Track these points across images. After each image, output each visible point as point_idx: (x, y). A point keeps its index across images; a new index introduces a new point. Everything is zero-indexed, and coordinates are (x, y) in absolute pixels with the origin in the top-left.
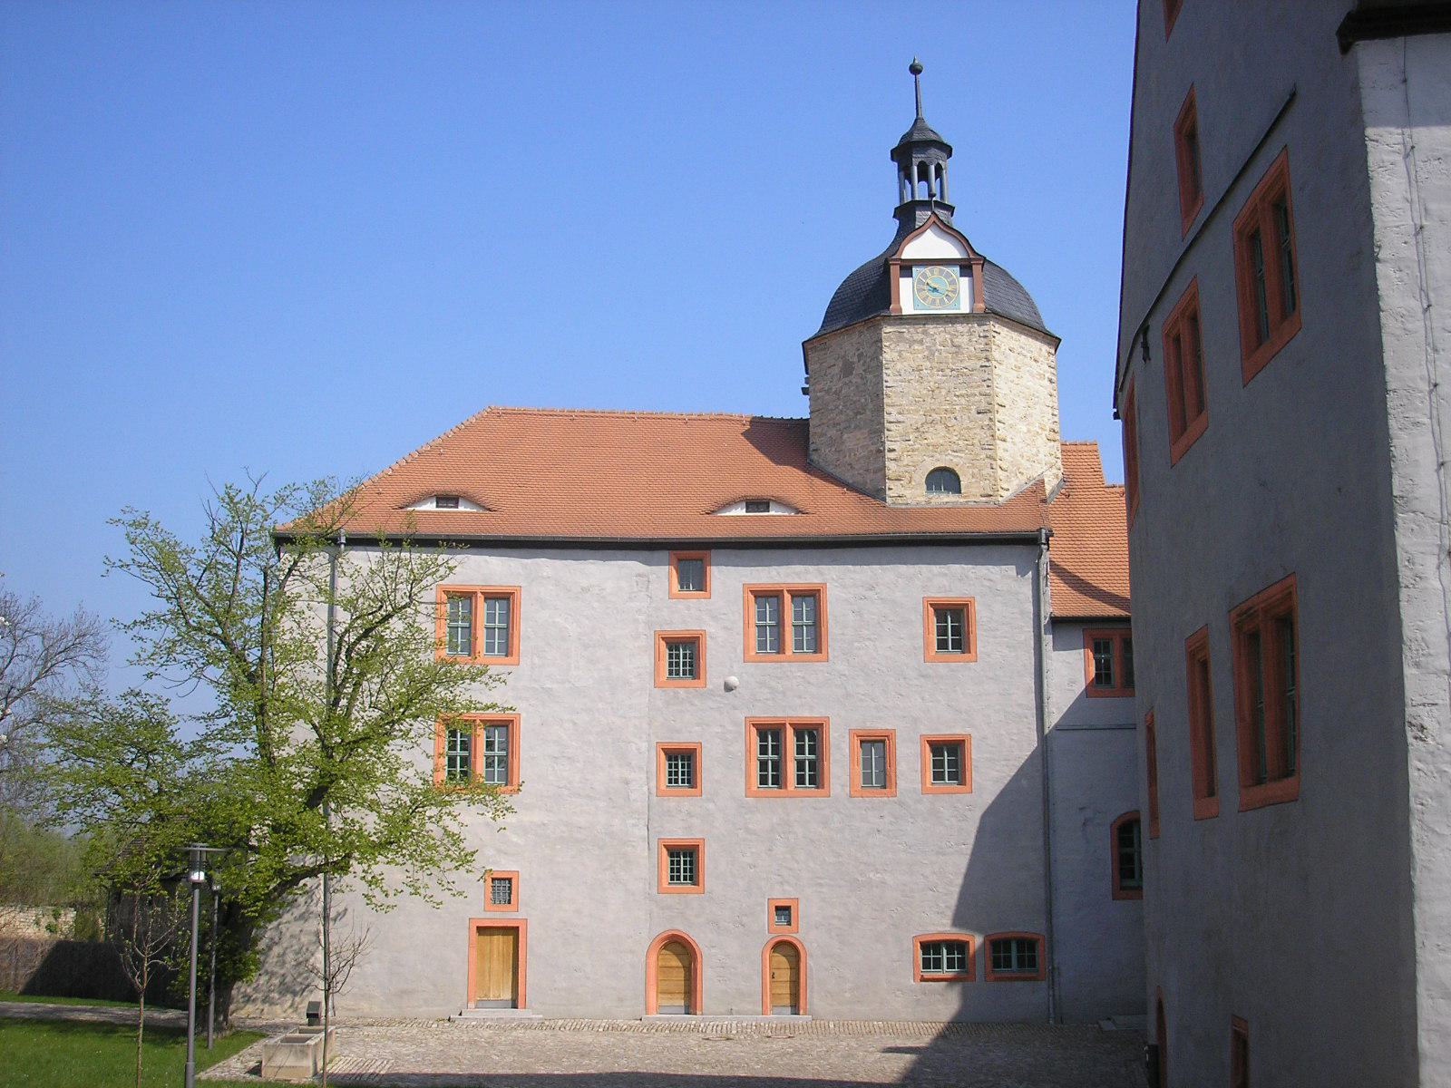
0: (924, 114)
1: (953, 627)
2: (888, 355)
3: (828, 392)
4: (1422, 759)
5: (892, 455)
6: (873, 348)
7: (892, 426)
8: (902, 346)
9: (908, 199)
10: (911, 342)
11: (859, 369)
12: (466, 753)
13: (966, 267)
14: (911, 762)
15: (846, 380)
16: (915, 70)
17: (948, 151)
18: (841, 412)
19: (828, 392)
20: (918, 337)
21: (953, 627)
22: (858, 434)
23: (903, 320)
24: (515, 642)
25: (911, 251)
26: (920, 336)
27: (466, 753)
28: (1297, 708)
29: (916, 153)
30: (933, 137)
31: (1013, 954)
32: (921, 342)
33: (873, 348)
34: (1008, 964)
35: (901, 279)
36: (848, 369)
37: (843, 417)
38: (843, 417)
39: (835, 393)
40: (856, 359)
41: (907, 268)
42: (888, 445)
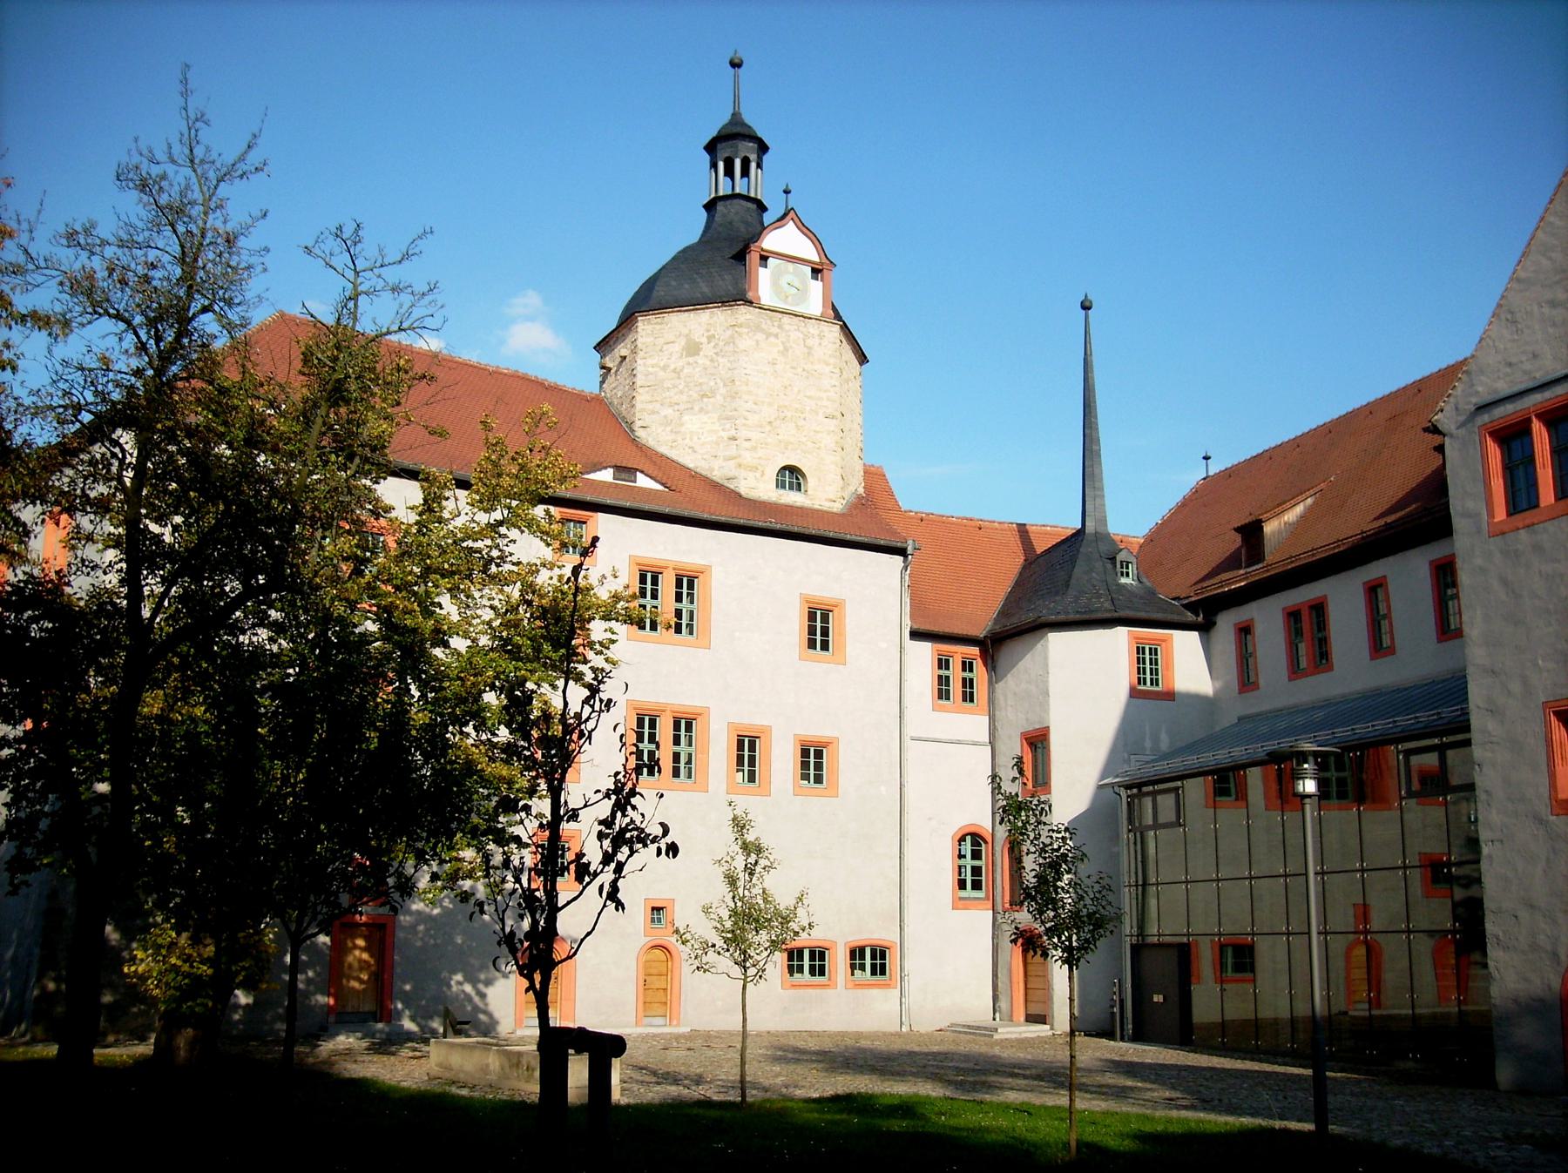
1: (819, 629)
3: (664, 368)
4: (1438, 913)
6: (729, 333)
8: (760, 336)
10: (768, 335)
11: (708, 350)
14: (781, 761)
15: (691, 360)
16: (1086, 307)
17: (763, 148)
18: (681, 392)
19: (664, 368)
20: (775, 330)
21: (819, 629)
22: (705, 418)
24: (1013, 1036)
26: (775, 330)
29: (734, 144)
32: (776, 336)
33: (729, 333)
34: (801, 969)
36: (693, 349)
37: (684, 398)
38: (684, 398)
39: (674, 371)
40: (704, 340)
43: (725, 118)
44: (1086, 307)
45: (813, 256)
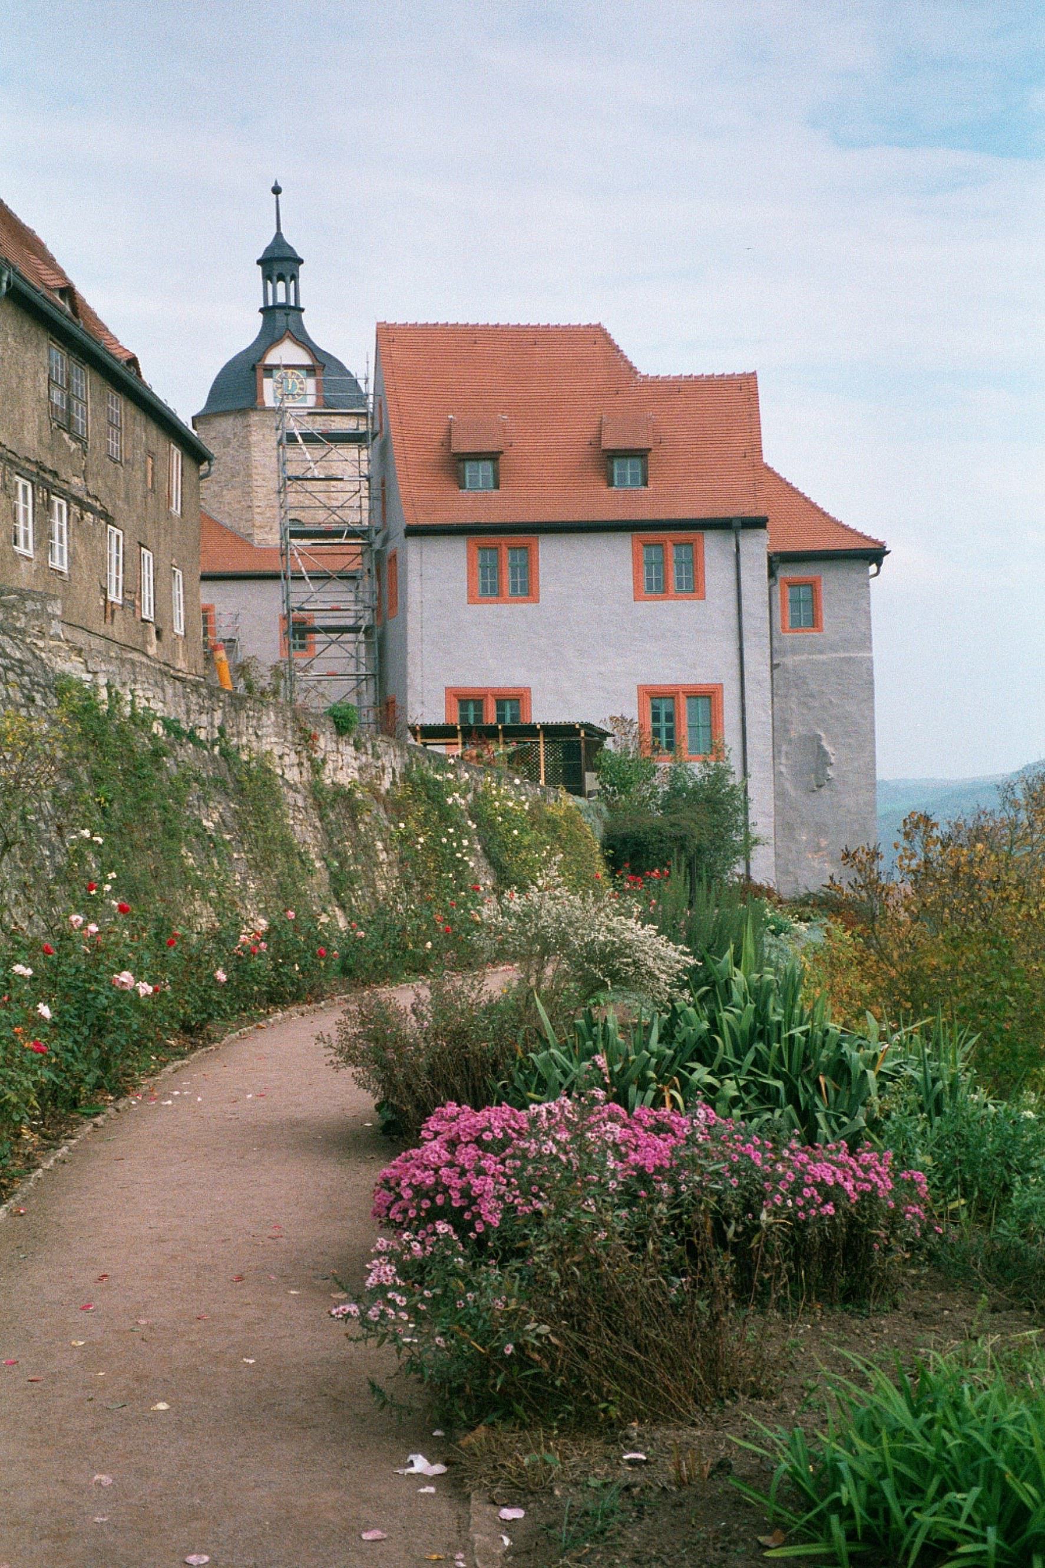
0: (282, 231)
2: (254, 438)
5: (258, 510)
7: (259, 490)
9: (270, 304)
11: (235, 443)
12: (670, 724)
13: (310, 370)
16: (277, 190)
23: (265, 410)
25: (272, 359)
27: (670, 724)
28: (688, 878)
29: (280, 263)
30: (289, 254)
31: (433, 1454)
35: (265, 380)
40: (232, 437)
41: (269, 370)
42: (256, 503)
43: (268, 240)
44: (277, 190)
45: (305, 359)
